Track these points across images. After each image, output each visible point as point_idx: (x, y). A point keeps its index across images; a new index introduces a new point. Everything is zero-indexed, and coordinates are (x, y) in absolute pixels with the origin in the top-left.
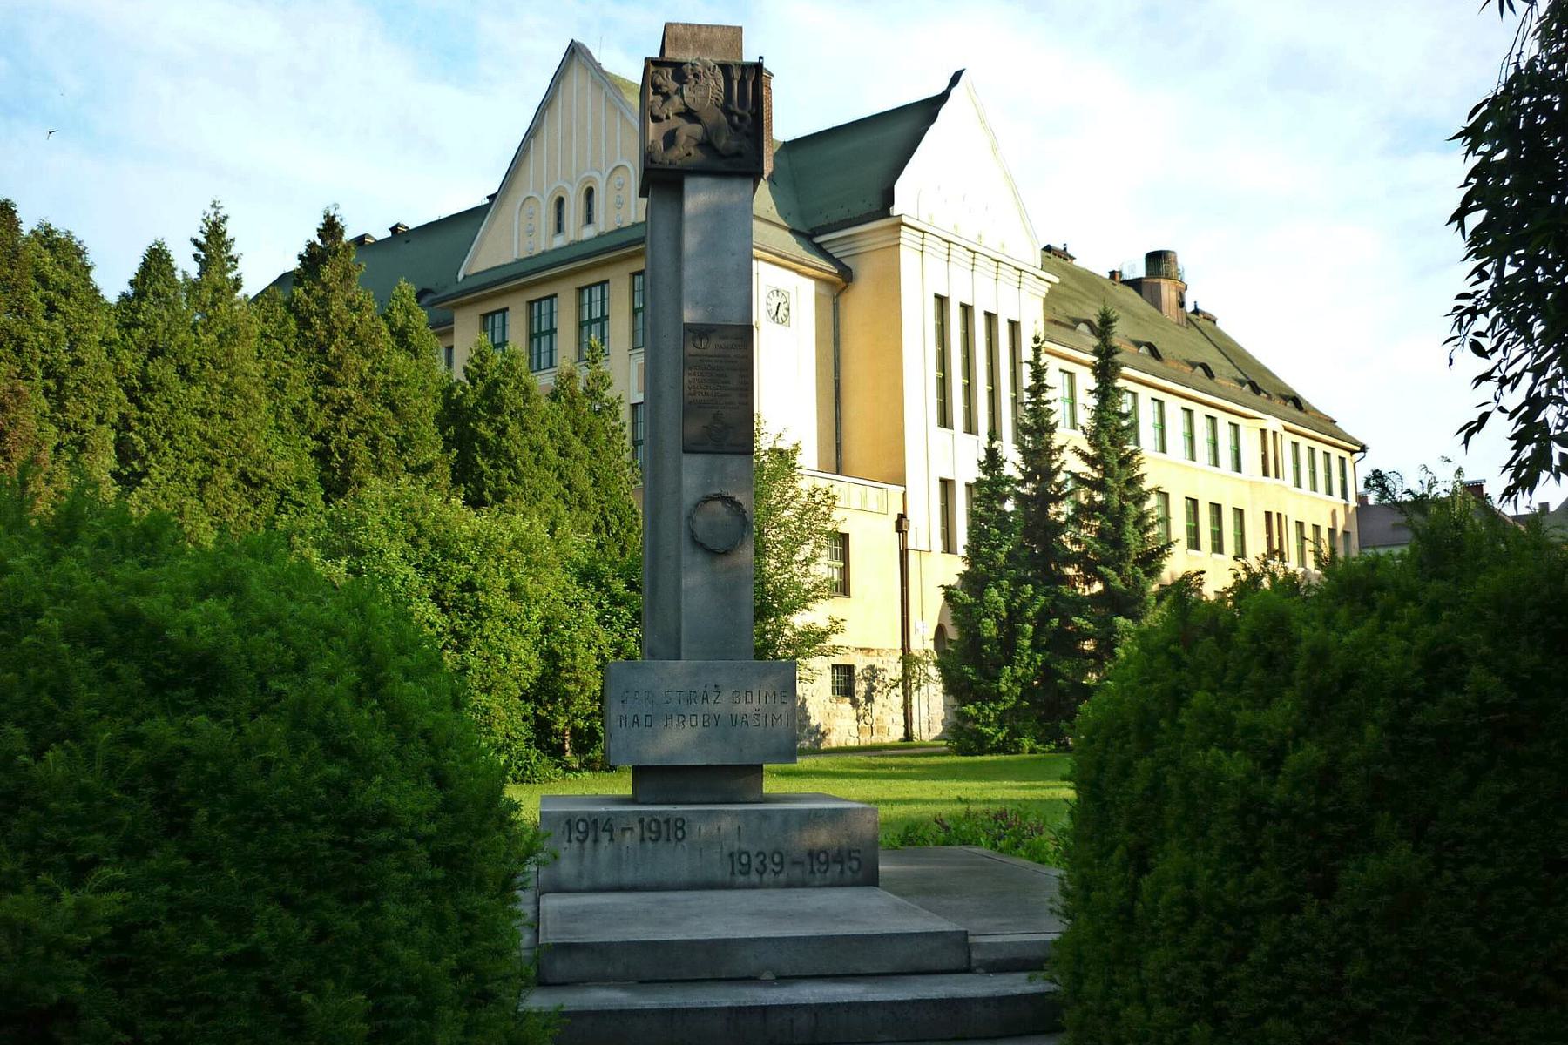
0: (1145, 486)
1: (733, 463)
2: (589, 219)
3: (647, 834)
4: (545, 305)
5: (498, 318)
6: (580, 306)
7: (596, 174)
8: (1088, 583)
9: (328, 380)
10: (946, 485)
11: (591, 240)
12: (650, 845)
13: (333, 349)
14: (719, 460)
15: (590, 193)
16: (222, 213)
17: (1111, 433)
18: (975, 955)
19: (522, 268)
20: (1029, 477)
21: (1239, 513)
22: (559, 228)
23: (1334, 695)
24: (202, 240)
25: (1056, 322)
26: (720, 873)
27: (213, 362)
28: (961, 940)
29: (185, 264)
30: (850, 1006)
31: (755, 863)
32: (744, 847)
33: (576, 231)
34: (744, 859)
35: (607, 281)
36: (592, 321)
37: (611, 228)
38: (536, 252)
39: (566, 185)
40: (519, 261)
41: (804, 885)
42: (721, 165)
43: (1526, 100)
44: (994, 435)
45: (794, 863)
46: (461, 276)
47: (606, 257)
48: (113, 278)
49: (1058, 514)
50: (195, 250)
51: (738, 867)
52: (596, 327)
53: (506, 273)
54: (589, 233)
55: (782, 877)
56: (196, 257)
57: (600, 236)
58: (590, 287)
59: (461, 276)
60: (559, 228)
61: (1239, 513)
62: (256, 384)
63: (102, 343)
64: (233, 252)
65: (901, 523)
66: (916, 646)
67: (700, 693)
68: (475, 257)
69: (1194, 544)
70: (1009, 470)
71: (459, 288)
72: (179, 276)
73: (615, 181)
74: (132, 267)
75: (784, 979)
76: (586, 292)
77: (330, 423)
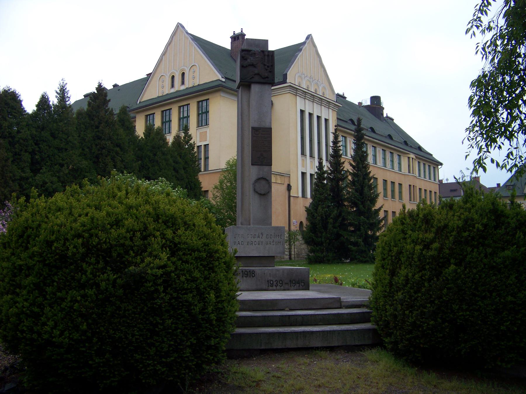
0: (371, 175)
1: (266, 168)
2: (183, 83)
3: (244, 275)
4: (168, 112)
5: (151, 116)
6: (179, 113)
7: (185, 68)
8: (352, 207)
9: (99, 138)
10: (303, 174)
11: (184, 90)
12: (245, 278)
13: (101, 127)
14: (262, 167)
15: (183, 74)
16: (65, 82)
17: (360, 158)
18: (342, 304)
19: (158, 100)
20: (333, 172)
21: (400, 185)
22: (173, 86)
23: (442, 230)
24: (59, 91)
25: (340, 120)
26: (265, 287)
27: (62, 131)
28: (338, 300)
29: (53, 100)
30: (311, 315)
31: (275, 283)
32: (271, 278)
33: (178, 87)
34: (272, 282)
35: (189, 104)
36: (184, 118)
37: (191, 86)
38: (164, 94)
39: (175, 72)
40: (159, 97)
41: (288, 290)
42: (262, 81)
43: (448, 340)
44: (320, 159)
45: (286, 283)
46: (138, 102)
47: (383, 143)
48: (30, 106)
49: (342, 184)
50: (56, 94)
51: (270, 284)
52: (185, 120)
53: (154, 101)
54: (183, 88)
55: (282, 287)
56: (56, 97)
57: (187, 89)
58: (183, 106)
59: (138, 102)
60: (173, 86)
61: (400, 185)
62: (76, 139)
63: (27, 125)
64: (69, 95)
65: (289, 187)
66: (293, 228)
67: (257, 235)
68: (142, 97)
69: (385, 196)
70: (325, 169)
71: (138, 106)
72: (51, 103)
73: (192, 70)
74: (37, 100)
75: (291, 310)
76: (182, 108)
77: (100, 152)
